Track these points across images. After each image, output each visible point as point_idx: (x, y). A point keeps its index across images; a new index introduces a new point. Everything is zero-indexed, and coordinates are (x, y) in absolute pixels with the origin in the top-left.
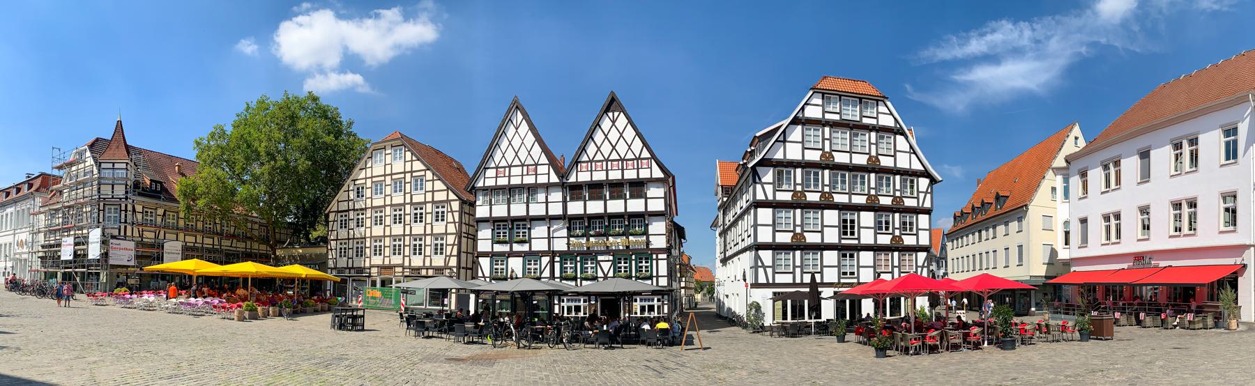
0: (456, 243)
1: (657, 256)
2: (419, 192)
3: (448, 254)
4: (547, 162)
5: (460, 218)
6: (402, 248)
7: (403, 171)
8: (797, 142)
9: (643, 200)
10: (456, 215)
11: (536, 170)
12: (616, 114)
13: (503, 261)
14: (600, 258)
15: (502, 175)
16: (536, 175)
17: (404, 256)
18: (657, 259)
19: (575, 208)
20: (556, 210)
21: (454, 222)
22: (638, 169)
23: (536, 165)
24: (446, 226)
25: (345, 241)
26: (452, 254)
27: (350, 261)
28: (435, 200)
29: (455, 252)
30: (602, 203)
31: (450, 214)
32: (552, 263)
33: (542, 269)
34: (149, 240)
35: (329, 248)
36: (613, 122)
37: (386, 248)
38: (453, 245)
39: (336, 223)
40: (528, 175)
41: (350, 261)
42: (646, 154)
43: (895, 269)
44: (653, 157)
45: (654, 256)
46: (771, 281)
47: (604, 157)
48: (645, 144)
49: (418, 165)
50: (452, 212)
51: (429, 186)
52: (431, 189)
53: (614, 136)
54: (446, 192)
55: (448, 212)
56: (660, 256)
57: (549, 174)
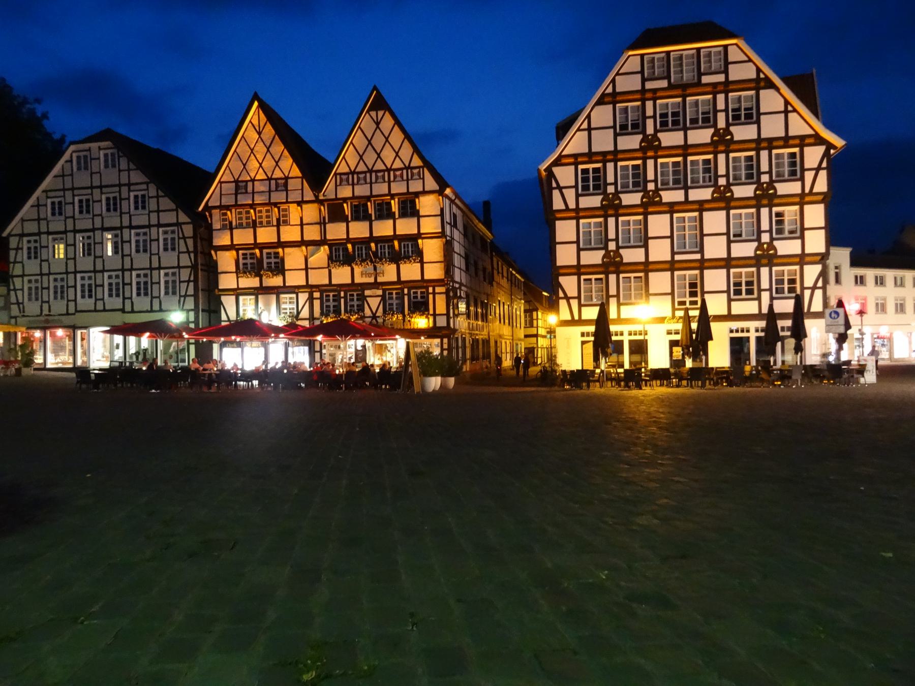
0: (192, 279)
1: (434, 290)
2: (140, 211)
3: (183, 293)
4: (300, 175)
5: (195, 246)
6: (66, 289)
7: (62, 187)
8: (64, 184)
9: (415, 219)
10: (190, 242)
11: (286, 185)
12: (380, 113)
13: (414, 297)
14: (367, 293)
15: (244, 191)
16: (287, 190)
17: (124, 298)
18: (434, 293)
19: (336, 231)
20: (312, 233)
21: (188, 252)
22: (371, 183)
23: (253, 180)
24: (178, 256)
25: (89, 274)
26: (188, 294)
27: (45, 306)
28: (77, 228)
29: (191, 291)
30: (367, 224)
31: (182, 241)
32: (311, 299)
33: (300, 309)
34: (11, 269)
35: (12, 287)
36: (378, 124)
37: (126, 287)
38: (189, 281)
39: (20, 251)
40: (276, 190)
41: (45, 306)
42: (416, 162)
43: (763, 293)
44: (427, 164)
45: (431, 290)
46: (576, 317)
47: (404, 165)
48: (416, 150)
49: (137, 177)
50: (184, 238)
51: (153, 204)
52: (156, 209)
53: (378, 141)
54: (175, 212)
55: (179, 238)
56: (438, 290)
57: (302, 189)
